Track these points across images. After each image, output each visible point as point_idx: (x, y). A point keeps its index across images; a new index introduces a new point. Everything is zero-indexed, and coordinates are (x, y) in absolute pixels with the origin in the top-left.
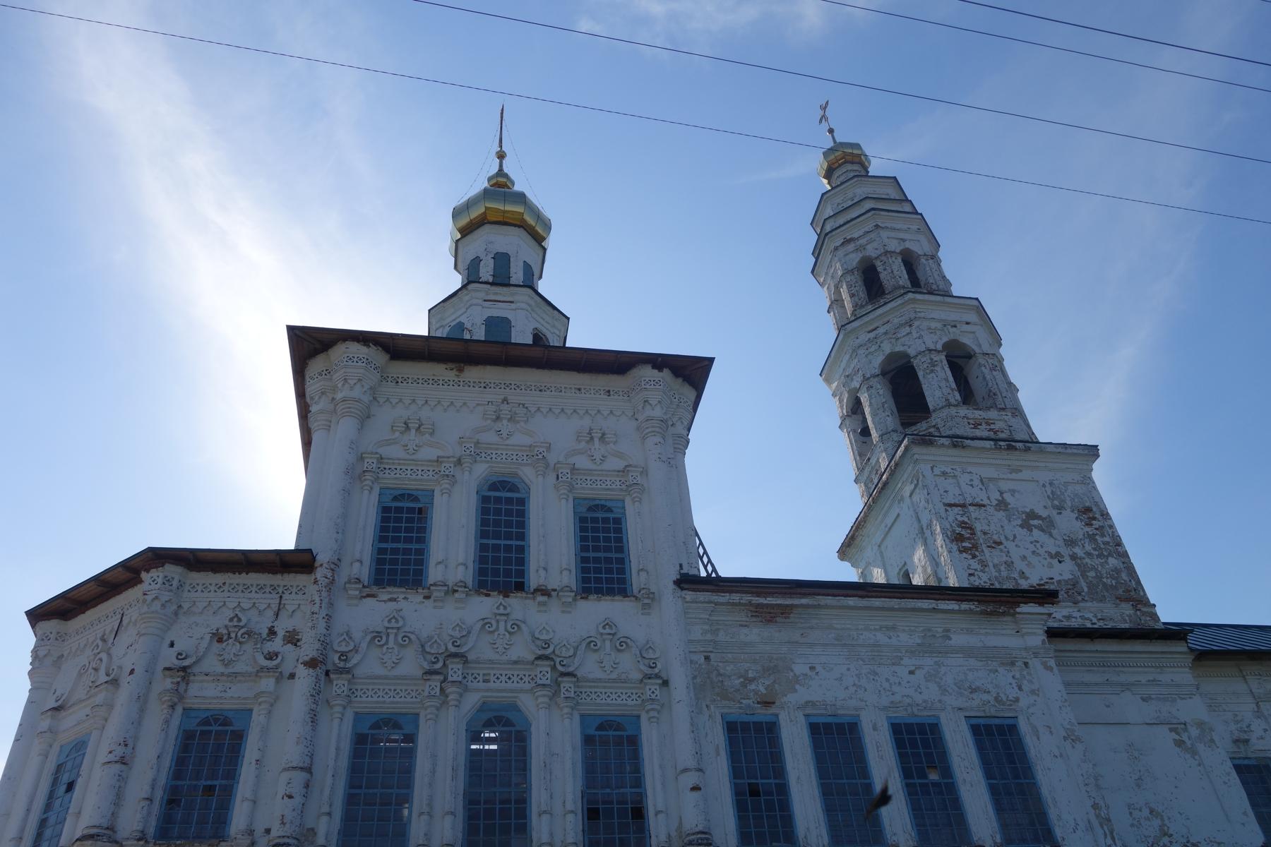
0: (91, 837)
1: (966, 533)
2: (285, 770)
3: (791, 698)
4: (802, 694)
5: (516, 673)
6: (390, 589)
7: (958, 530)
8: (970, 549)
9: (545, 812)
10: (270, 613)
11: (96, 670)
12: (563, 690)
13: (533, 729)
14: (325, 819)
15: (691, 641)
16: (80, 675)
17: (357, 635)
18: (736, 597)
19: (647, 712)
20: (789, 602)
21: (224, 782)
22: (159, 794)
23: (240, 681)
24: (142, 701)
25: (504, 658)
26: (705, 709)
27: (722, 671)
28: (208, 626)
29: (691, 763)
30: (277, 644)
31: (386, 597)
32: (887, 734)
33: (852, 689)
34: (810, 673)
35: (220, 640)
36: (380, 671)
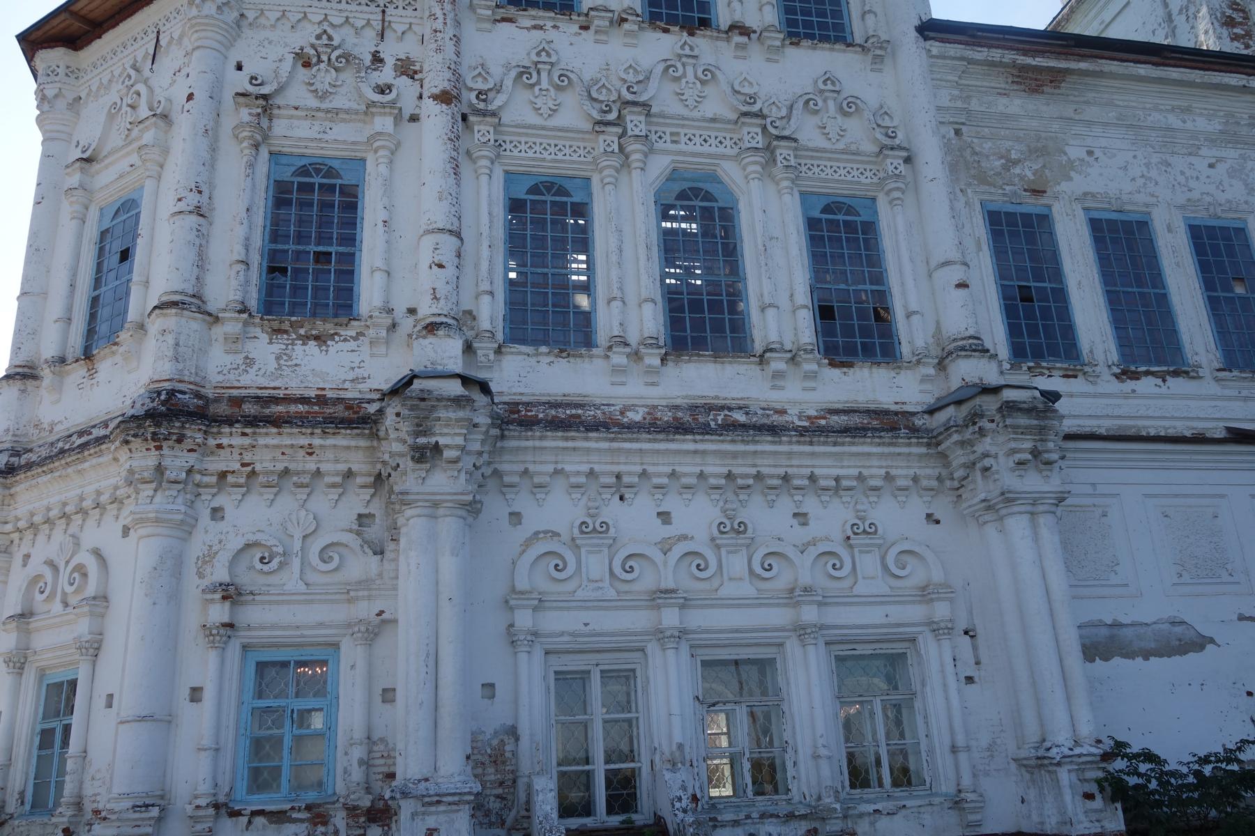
0: (174, 304)
1: (1238, 17)
2: (428, 232)
3: (1064, 186)
4: (1077, 184)
5: (713, 134)
6: (533, 12)
7: (1229, 12)
8: (1243, 37)
9: (770, 305)
10: (370, 34)
11: (133, 107)
12: (779, 158)
13: (742, 206)
14: (486, 299)
15: (939, 108)
16: (111, 117)
17: (496, 71)
18: (996, 54)
19: (888, 193)
20: (1063, 64)
21: (341, 249)
22: (255, 259)
23: (343, 120)
24: (211, 134)
25: (695, 114)
26: (959, 194)
27: (978, 149)
28: (286, 45)
29: (954, 255)
30: (386, 75)
31: (529, 23)
32: (1184, 237)
33: (1140, 182)
34: (1087, 158)
35: (307, 65)
36: (533, 119)
